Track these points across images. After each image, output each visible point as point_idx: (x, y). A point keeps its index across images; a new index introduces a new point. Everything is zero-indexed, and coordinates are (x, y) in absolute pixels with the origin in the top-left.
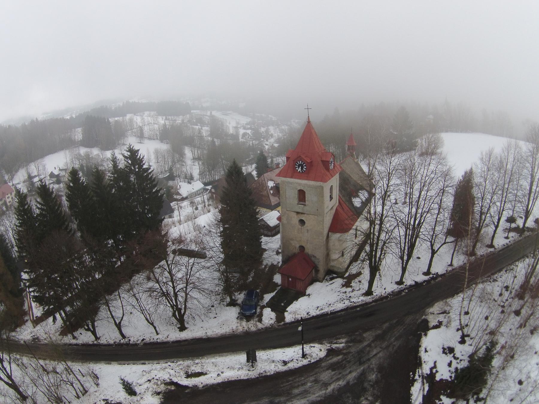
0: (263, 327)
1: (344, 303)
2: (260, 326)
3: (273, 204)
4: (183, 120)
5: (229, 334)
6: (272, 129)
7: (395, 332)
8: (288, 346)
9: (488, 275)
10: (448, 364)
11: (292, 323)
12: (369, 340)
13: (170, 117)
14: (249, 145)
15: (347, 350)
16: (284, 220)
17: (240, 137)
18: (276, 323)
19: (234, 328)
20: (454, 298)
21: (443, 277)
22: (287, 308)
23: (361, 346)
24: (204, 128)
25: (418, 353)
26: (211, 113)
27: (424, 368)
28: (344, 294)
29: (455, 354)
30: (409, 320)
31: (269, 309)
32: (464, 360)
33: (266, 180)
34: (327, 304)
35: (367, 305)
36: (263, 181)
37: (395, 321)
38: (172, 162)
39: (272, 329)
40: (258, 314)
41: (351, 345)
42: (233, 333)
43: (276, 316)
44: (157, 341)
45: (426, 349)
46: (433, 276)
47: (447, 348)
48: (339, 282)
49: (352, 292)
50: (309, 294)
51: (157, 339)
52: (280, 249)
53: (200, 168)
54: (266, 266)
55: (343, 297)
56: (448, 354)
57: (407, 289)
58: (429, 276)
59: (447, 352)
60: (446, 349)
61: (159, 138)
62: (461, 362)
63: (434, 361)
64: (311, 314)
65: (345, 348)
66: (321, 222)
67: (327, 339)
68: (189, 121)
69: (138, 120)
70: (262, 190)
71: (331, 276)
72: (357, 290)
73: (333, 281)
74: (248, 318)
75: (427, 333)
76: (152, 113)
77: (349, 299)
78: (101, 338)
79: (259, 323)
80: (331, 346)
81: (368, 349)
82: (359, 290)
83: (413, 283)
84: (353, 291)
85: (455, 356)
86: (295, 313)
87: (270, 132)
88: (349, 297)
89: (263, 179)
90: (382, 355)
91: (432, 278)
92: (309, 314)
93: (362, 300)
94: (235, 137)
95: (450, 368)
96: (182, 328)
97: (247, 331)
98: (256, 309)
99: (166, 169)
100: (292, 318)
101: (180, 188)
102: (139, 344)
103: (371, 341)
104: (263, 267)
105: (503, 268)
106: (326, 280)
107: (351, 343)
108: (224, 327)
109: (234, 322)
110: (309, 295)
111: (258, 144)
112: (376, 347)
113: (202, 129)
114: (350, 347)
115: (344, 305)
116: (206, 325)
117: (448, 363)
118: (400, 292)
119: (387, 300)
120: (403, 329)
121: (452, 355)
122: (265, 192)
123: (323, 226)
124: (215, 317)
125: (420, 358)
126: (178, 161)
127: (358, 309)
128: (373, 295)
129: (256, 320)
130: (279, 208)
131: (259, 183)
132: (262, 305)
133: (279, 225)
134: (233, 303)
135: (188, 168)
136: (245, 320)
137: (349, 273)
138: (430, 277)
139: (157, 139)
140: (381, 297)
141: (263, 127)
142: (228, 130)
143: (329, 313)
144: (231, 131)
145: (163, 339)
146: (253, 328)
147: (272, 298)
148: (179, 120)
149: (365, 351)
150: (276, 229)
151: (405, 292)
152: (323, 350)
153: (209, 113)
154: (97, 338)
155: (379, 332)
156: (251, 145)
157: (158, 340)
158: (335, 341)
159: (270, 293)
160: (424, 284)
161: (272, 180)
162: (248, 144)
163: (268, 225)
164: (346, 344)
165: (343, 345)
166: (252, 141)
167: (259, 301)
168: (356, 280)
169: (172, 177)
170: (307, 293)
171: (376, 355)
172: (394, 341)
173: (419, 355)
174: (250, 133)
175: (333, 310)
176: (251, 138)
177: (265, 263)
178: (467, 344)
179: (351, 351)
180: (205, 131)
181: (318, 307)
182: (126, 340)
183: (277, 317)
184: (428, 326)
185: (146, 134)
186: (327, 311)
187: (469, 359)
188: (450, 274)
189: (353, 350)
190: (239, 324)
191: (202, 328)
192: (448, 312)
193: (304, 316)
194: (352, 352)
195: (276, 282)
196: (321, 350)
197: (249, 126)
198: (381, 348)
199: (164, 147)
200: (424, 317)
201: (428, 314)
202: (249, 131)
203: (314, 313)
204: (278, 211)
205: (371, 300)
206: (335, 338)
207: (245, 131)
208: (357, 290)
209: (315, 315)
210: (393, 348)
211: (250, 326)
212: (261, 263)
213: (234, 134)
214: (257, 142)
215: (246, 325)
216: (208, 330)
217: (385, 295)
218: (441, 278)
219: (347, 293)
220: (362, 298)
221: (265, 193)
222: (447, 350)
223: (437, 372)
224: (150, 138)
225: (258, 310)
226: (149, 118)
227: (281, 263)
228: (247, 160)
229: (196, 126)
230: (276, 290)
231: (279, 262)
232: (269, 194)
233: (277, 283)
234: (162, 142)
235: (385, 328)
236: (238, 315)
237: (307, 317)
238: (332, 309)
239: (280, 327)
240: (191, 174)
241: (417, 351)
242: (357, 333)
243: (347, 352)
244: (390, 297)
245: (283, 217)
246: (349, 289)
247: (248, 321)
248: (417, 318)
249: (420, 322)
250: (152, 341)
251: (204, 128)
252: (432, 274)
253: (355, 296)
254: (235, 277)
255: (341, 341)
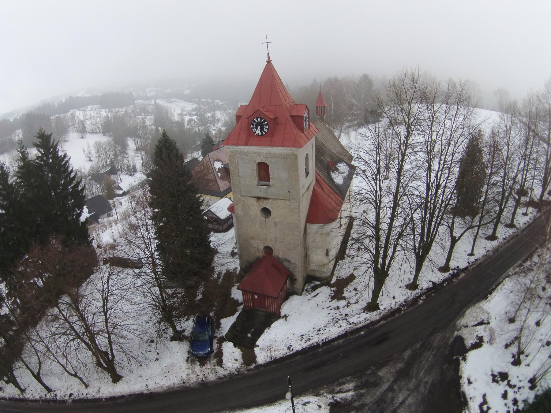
0: (226, 373)
1: (341, 326)
2: (221, 372)
3: (222, 190)
4: (126, 111)
5: (179, 387)
6: (218, 114)
7: (423, 363)
8: (269, 403)
9: (519, 263)
10: (501, 395)
11: (267, 364)
12: (388, 381)
13: (113, 109)
14: (195, 130)
15: (359, 401)
16: (239, 211)
17: (186, 124)
18: (243, 366)
19: (185, 377)
20: (489, 301)
21: (466, 272)
22: (256, 340)
23: (379, 392)
24: (147, 117)
25: (460, 388)
26: (155, 101)
27: (472, 408)
28: (336, 311)
29: (509, 381)
30: (437, 340)
31: (231, 344)
32: (524, 387)
33: (212, 161)
34: (315, 329)
35: (374, 325)
36: (208, 162)
37: (418, 345)
38: (114, 155)
39: (239, 377)
40: (215, 351)
41: (364, 393)
42: (184, 385)
43: (242, 355)
44: (88, 397)
45: (469, 380)
46: (454, 272)
47: (498, 374)
48: (325, 292)
49: (348, 306)
50: (285, 315)
51: (87, 394)
52: (236, 248)
53: (142, 159)
54: (219, 275)
55: (335, 315)
56: (501, 382)
57: (424, 294)
58: (449, 273)
59: (499, 379)
60: (496, 376)
61: (101, 131)
62: (520, 390)
63: (483, 394)
64: (294, 349)
65: (356, 398)
66: (296, 210)
67: (325, 386)
68: (133, 111)
69: (79, 114)
70: (207, 174)
71: (312, 285)
72: (355, 303)
73: (317, 291)
74: (203, 361)
75: (466, 356)
76: (96, 106)
77: (346, 319)
78: (27, 389)
79: (219, 368)
80: (333, 397)
81: (390, 395)
82: (357, 303)
83: (430, 285)
84: (349, 304)
85: (511, 383)
86: (269, 348)
87: (217, 117)
88: (344, 315)
89: (207, 159)
90: (412, 401)
91: (454, 275)
92: (291, 348)
93: (365, 319)
94: (180, 124)
95: (506, 401)
96: (116, 378)
97: (203, 381)
98: (211, 345)
99: (108, 163)
100: (266, 358)
101: (121, 181)
102: (67, 400)
103: (391, 381)
104: (216, 276)
105: (534, 252)
106: (306, 290)
107: (362, 389)
108: (170, 376)
109: (184, 368)
110: (285, 317)
111: (204, 129)
112: (401, 390)
113: (146, 118)
114: (362, 395)
115: (341, 329)
116: (146, 372)
117: (502, 394)
118: (416, 299)
119: (400, 314)
120: (432, 356)
121: (506, 382)
122: (212, 175)
123: (299, 216)
124: (157, 359)
125: (464, 394)
126: (121, 153)
127: (362, 333)
128: (379, 309)
129: (213, 363)
130: (231, 195)
131: (203, 165)
132: (219, 336)
133: (232, 217)
134: (178, 337)
135: (130, 159)
136: (198, 363)
137: (337, 277)
138: (450, 274)
139: (100, 132)
140: (392, 310)
141: (210, 112)
142: (172, 118)
143: (321, 343)
144: (176, 118)
145: (94, 394)
146: (211, 375)
147: (233, 326)
148: (122, 111)
149: (386, 400)
150: (229, 222)
151: (422, 300)
152: (323, 406)
153: (153, 102)
154: (23, 391)
155: (400, 365)
156: (197, 131)
157: (88, 396)
158: (338, 389)
159: (229, 316)
160: (445, 285)
161: (219, 160)
162: (194, 130)
163: (218, 218)
164: (357, 392)
165: (351, 393)
166: (198, 127)
167: (215, 331)
168: (350, 287)
169: (113, 171)
170: (282, 314)
171: (403, 402)
172: (425, 377)
173: (461, 390)
174: (196, 119)
175: (326, 338)
176: (196, 124)
177: (218, 269)
178: (523, 365)
179: (366, 403)
180: (149, 121)
181: (303, 335)
182: (52, 395)
183: (244, 356)
184: (464, 346)
185: (88, 129)
186: (316, 340)
187: (530, 385)
188: (474, 266)
189: (369, 400)
190: (190, 371)
191: (141, 378)
192: (487, 322)
193: (284, 352)
194: (368, 404)
195: (235, 299)
196: (320, 407)
197: (194, 113)
198: (408, 390)
199: (104, 139)
200: (456, 333)
201: (461, 328)
202: (195, 118)
203: (298, 346)
204: (229, 198)
205: (378, 318)
206: (336, 383)
207: (190, 117)
208: (355, 303)
209: (300, 349)
210: (425, 387)
211: (206, 373)
212: (213, 270)
213: (180, 121)
214: (203, 128)
215: (201, 372)
216: (149, 381)
217: (396, 307)
218: (464, 273)
219: (341, 309)
220: (364, 316)
221: (211, 177)
222: (498, 377)
223: (489, 408)
224: (92, 132)
225: (215, 346)
226: (92, 112)
227: (239, 269)
228: (194, 146)
229: (140, 116)
230: (237, 311)
231: (236, 268)
232: (216, 177)
233: (237, 300)
234: (104, 135)
235: (406, 357)
236: (188, 356)
237: (288, 354)
238: (324, 337)
239: (251, 372)
240: (134, 166)
241: (458, 385)
242: (368, 372)
243: (360, 405)
244: (403, 309)
245: (236, 207)
246: (342, 303)
247: (202, 364)
248: (448, 335)
249: (453, 341)
250: (81, 396)
251: (147, 117)
252: (452, 270)
253: (354, 314)
254: (180, 293)
255: (348, 387)
